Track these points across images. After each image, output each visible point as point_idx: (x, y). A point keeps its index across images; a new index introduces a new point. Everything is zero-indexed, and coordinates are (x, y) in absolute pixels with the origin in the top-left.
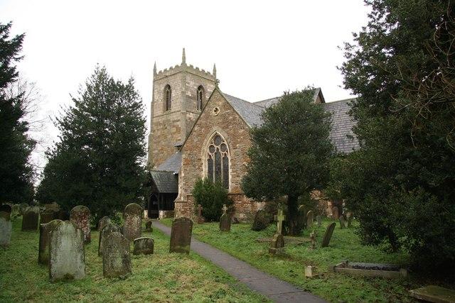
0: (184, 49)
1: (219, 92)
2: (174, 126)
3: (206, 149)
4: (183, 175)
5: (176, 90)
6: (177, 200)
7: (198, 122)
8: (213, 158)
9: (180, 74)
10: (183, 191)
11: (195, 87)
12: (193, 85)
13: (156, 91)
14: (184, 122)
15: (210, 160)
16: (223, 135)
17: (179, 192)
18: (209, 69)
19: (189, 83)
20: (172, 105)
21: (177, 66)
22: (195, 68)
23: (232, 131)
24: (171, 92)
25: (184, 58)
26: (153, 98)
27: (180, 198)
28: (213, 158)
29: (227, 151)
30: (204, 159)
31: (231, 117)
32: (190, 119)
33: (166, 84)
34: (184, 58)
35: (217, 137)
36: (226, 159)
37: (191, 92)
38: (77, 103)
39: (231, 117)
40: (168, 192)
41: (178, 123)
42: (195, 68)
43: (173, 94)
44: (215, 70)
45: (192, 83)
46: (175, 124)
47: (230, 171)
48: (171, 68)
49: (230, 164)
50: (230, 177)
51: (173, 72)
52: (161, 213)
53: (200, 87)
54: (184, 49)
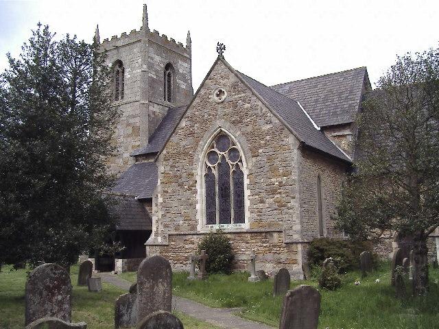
0: (145, 7)
1: (226, 64)
2: (128, 125)
3: (201, 156)
4: (160, 200)
5: (133, 69)
6: (150, 240)
7: (188, 114)
8: (215, 172)
9: (138, 44)
10: (161, 228)
11: (163, 66)
12: (159, 61)
14: (146, 119)
15: (209, 176)
16: (234, 135)
17: (154, 229)
18: (181, 39)
19: (152, 59)
20: (126, 92)
21: (134, 32)
22: (161, 35)
23: (249, 129)
24: (123, 72)
25: (145, 18)
27: (156, 239)
28: (215, 172)
29: (241, 161)
30: (200, 174)
31: (247, 105)
32: (154, 113)
33: (115, 59)
34: (145, 18)
35: (221, 138)
36: (239, 174)
37: (157, 71)
38: (96, 39)
39: (247, 105)
41: (137, 120)
42: (161, 35)
43: (127, 75)
44: (189, 41)
45: (157, 58)
46: (131, 121)
47: (247, 193)
48: (124, 35)
49: (246, 182)
50: (247, 203)
51: (127, 41)
52: (119, 263)
53: (168, 66)
54: (145, 7)
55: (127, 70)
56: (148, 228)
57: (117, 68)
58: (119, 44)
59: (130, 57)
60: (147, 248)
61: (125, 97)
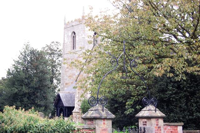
6: (74, 111)
10: (77, 106)
13: (66, 35)
20: (77, 46)
26: (64, 40)
40: (70, 106)
55: (77, 36)
56: (74, 106)
57: (73, 35)
58: (74, 24)
59: (78, 31)
60: (73, 113)
61: (76, 48)
